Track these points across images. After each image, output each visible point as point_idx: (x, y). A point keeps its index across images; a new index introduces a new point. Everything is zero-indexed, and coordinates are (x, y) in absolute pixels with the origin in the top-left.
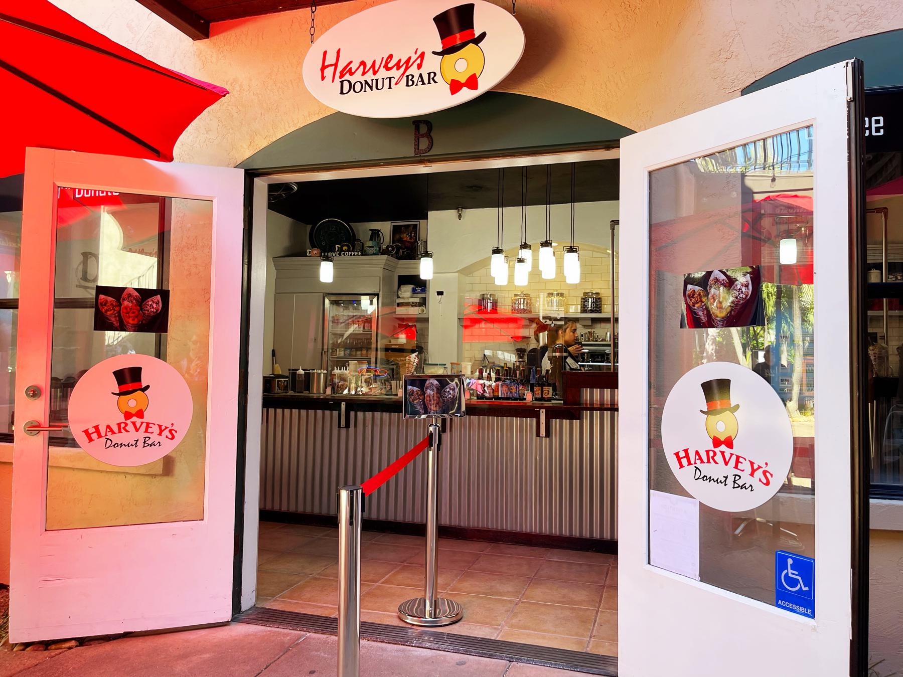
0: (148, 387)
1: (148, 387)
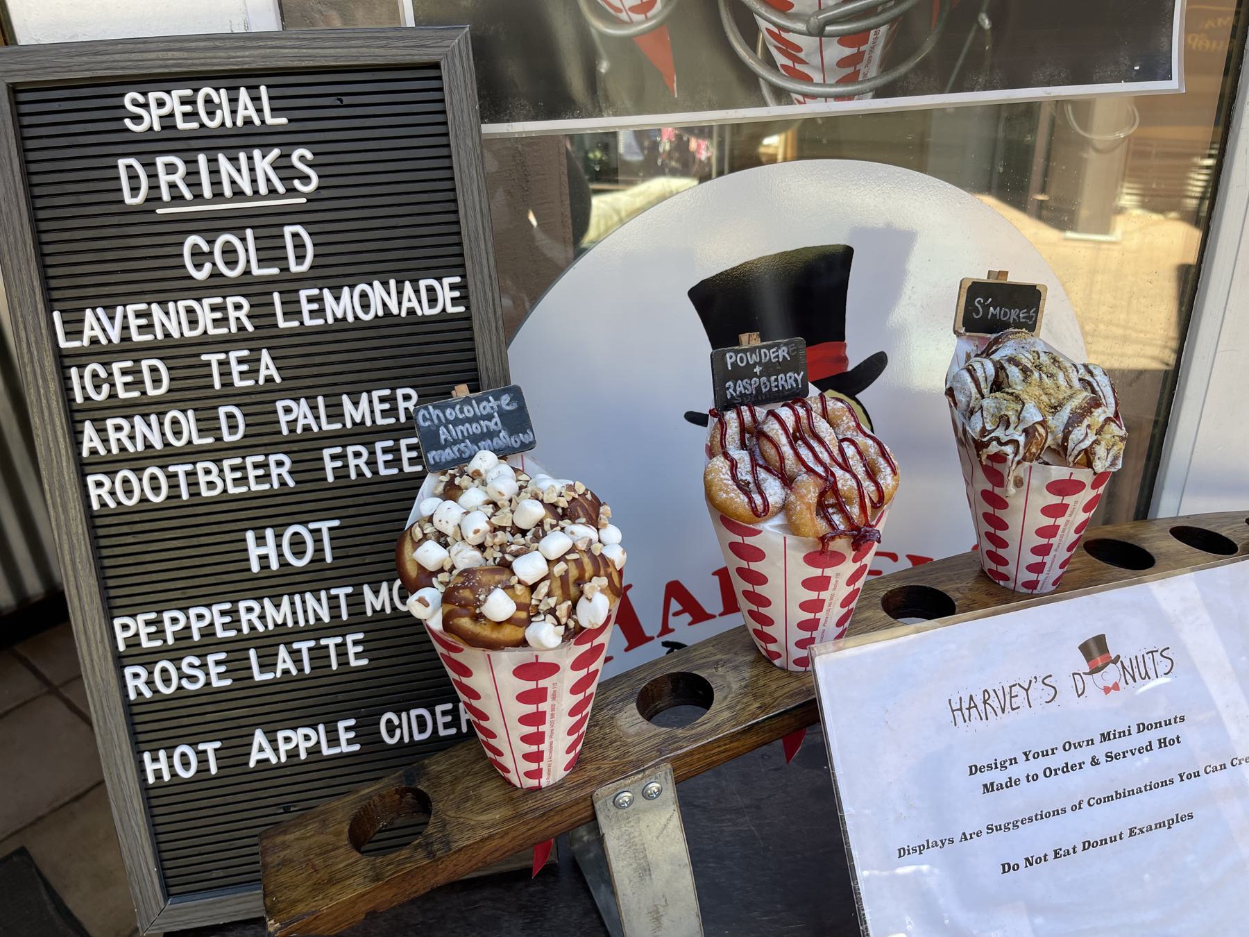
0: (876, 364)
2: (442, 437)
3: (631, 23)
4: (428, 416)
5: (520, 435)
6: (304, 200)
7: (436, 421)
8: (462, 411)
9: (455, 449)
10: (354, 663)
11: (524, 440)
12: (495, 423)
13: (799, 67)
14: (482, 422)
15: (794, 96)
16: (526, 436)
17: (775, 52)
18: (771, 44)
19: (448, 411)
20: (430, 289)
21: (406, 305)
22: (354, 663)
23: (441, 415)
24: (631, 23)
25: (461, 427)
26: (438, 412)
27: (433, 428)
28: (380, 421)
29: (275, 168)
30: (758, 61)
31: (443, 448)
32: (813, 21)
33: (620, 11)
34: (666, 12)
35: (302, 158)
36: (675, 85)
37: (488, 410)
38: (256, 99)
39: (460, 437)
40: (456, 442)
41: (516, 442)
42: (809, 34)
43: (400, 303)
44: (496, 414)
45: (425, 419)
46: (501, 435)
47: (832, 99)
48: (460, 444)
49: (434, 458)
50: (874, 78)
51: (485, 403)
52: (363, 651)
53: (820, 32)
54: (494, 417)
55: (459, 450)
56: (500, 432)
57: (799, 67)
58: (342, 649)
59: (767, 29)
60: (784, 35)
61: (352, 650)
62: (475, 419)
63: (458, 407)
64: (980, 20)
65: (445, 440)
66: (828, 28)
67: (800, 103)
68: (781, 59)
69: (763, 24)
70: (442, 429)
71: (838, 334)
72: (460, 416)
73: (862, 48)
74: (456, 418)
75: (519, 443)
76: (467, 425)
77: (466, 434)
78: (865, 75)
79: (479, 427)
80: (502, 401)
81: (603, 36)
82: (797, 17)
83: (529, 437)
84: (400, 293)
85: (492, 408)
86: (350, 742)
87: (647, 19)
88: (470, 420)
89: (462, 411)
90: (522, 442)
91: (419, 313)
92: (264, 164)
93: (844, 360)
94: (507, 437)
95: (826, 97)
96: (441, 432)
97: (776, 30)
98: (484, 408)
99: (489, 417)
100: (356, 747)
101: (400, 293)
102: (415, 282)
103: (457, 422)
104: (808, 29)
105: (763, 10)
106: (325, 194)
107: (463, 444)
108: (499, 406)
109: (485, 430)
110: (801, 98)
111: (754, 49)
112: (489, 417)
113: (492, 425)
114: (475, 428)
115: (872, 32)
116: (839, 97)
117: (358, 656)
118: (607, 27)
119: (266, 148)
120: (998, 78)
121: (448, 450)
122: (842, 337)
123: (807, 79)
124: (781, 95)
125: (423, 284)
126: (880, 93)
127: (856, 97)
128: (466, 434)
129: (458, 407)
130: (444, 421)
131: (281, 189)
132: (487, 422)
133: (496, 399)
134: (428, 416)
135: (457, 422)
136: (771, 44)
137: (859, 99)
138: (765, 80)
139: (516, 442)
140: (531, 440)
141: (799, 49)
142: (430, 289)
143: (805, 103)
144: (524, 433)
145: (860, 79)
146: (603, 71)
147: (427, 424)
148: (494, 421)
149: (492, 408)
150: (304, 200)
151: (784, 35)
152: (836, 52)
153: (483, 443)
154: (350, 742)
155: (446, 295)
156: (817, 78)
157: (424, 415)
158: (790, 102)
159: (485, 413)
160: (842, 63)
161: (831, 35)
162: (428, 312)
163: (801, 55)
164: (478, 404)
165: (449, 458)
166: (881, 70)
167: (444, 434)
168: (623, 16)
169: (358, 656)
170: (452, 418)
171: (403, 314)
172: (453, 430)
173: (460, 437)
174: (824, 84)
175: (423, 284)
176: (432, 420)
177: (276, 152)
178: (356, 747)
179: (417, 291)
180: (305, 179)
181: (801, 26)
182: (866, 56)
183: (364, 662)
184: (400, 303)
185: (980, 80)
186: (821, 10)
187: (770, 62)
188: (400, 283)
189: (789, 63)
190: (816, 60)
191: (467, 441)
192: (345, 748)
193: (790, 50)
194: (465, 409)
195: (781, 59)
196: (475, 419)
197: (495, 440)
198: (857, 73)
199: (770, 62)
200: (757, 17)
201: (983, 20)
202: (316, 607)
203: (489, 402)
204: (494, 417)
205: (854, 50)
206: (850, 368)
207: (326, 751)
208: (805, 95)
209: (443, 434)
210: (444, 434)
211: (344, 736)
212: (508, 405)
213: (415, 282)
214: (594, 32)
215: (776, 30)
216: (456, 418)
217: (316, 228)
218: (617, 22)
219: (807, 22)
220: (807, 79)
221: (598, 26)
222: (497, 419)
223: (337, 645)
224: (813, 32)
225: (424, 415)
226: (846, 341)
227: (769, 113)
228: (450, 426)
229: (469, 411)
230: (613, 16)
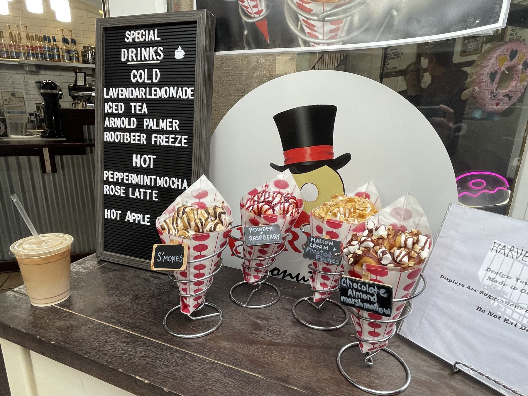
0: (345, 159)
1: (345, 159)
2: (349, 293)
3: (255, 18)
4: (346, 282)
5: (384, 309)
6: (159, 62)
7: (348, 286)
8: (361, 287)
9: (353, 300)
10: (154, 199)
11: (385, 312)
12: (374, 299)
13: (314, 33)
14: (368, 295)
15: (311, 43)
16: (387, 311)
17: (305, 27)
18: (303, 24)
19: (355, 284)
20: (186, 91)
21: (178, 95)
22: (154, 199)
23: (351, 284)
24: (255, 18)
25: (358, 293)
26: (350, 282)
27: (347, 288)
28: (168, 129)
29: (155, 53)
30: (299, 31)
31: (349, 297)
32: (321, 16)
33: (251, 14)
34: (266, 13)
35: (160, 50)
36: (268, 39)
37: (373, 292)
38: (154, 33)
39: (357, 297)
40: (354, 298)
41: (381, 311)
42: (319, 20)
43: (177, 94)
44: (376, 295)
45: (344, 283)
46: (375, 305)
47: (326, 45)
48: (356, 299)
49: (343, 299)
50: (344, 37)
51: (372, 288)
52: (157, 197)
53: (323, 20)
54: (374, 296)
55: (354, 301)
56: (375, 303)
57: (314, 33)
58: (151, 194)
59: (302, 19)
60: (309, 21)
61: (154, 195)
62: (365, 292)
63: (359, 284)
64: (392, 12)
65: (350, 295)
66: (326, 19)
67: (313, 46)
68: (307, 30)
69: (301, 17)
70: (350, 290)
71: (329, 142)
72: (359, 288)
73: (340, 26)
74: (357, 288)
75: (382, 312)
76: (361, 293)
77: (359, 297)
78: (340, 36)
79: (366, 297)
80: (381, 291)
81: (246, 22)
82: (314, 15)
83: (389, 312)
84: (177, 91)
85: (375, 291)
86: (148, 222)
87: (260, 16)
88: (364, 292)
89: (361, 287)
90: (357, 284)
91: (182, 97)
92: (152, 50)
93: (332, 154)
94: (378, 307)
95: (323, 44)
96: (349, 291)
97: (306, 19)
98: (371, 290)
99: (372, 295)
100: (149, 224)
101: (177, 91)
102: (182, 88)
103: (357, 290)
104: (318, 18)
105: (301, 13)
106: (166, 60)
107: (357, 300)
108: (378, 293)
109: (368, 299)
110: (314, 44)
111: (297, 27)
112: (372, 295)
113: (372, 299)
114: (364, 296)
115: (344, 19)
116: (328, 44)
117: (155, 197)
118: (247, 19)
119: (153, 47)
120: (399, 34)
121: (350, 299)
122: (332, 145)
123: (317, 37)
124: (306, 43)
125: (184, 89)
126: (344, 43)
127: (336, 44)
128: (359, 297)
129: (359, 284)
130: (352, 287)
131: (155, 58)
132: (370, 296)
133: (378, 289)
134: (346, 282)
135: (357, 290)
136: (303, 24)
137: (336, 45)
138: (300, 37)
139: (381, 311)
140: (389, 313)
141: (314, 26)
142: (186, 91)
143: (315, 46)
144: (387, 309)
145: (338, 37)
146: (245, 34)
147: (345, 285)
148: (374, 297)
149: (375, 291)
150: (159, 62)
151: (309, 21)
152: (329, 27)
153: (366, 304)
154: (148, 222)
155: (189, 93)
156: (321, 37)
157: (344, 281)
158: (310, 46)
159: (371, 292)
160: (331, 32)
161: (328, 21)
162: (185, 97)
163: (315, 29)
164: (369, 287)
165: (350, 303)
166: (347, 34)
167: (350, 292)
168: (252, 15)
169: (155, 197)
170: (356, 288)
171: (178, 97)
172: (354, 293)
173: (357, 297)
174: (323, 39)
175: (184, 89)
176: (347, 284)
177: (156, 48)
178: (149, 224)
179: (182, 91)
180: (160, 56)
181: (316, 18)
182: (341, 29)
183: (157, 200)
184: (177, 94)
185: (391, 36)
186: (324, 12)
187: (302, 31)
188: (178, 88)
189: (310, 31)
190: (321, 30)
191: (359, 300)
192: (146, 223)
193: (311, 27)
194: (363, 286)
195: (307, 30)
196: (365, 292)
197: (372, 305)
198: (336, 35)
199: (302, 31)
200: (298, 15)
201: (393, 12)
202: (147, 180)
203: (374, 288)
204: (374, 296)
205: (336, 26)
206: (334, 158)
207: (142, 223)
208: (315, 43)
209: (350, 292)
210: (350, 292)
211: (147, 220)
212: (383, 294)
213: (182, 88)
214: (243, 21)
215: (306, 19)
216: (357, 288)
217: (162, 70)
218: (249, 17)
219: (318, 16)
220: (317, 37)
221: (245, 19)
222: (375, 297)
223: (150, 193)
224: (320, 19)
225: (344, 281)
226: (333, 146)
227: (301, 49)
228: (354, 290)
229: (364, 288)
230: (249, 15)
